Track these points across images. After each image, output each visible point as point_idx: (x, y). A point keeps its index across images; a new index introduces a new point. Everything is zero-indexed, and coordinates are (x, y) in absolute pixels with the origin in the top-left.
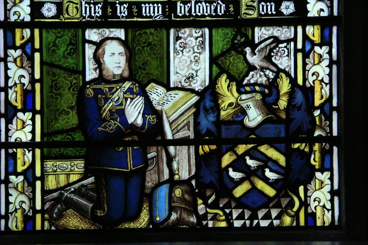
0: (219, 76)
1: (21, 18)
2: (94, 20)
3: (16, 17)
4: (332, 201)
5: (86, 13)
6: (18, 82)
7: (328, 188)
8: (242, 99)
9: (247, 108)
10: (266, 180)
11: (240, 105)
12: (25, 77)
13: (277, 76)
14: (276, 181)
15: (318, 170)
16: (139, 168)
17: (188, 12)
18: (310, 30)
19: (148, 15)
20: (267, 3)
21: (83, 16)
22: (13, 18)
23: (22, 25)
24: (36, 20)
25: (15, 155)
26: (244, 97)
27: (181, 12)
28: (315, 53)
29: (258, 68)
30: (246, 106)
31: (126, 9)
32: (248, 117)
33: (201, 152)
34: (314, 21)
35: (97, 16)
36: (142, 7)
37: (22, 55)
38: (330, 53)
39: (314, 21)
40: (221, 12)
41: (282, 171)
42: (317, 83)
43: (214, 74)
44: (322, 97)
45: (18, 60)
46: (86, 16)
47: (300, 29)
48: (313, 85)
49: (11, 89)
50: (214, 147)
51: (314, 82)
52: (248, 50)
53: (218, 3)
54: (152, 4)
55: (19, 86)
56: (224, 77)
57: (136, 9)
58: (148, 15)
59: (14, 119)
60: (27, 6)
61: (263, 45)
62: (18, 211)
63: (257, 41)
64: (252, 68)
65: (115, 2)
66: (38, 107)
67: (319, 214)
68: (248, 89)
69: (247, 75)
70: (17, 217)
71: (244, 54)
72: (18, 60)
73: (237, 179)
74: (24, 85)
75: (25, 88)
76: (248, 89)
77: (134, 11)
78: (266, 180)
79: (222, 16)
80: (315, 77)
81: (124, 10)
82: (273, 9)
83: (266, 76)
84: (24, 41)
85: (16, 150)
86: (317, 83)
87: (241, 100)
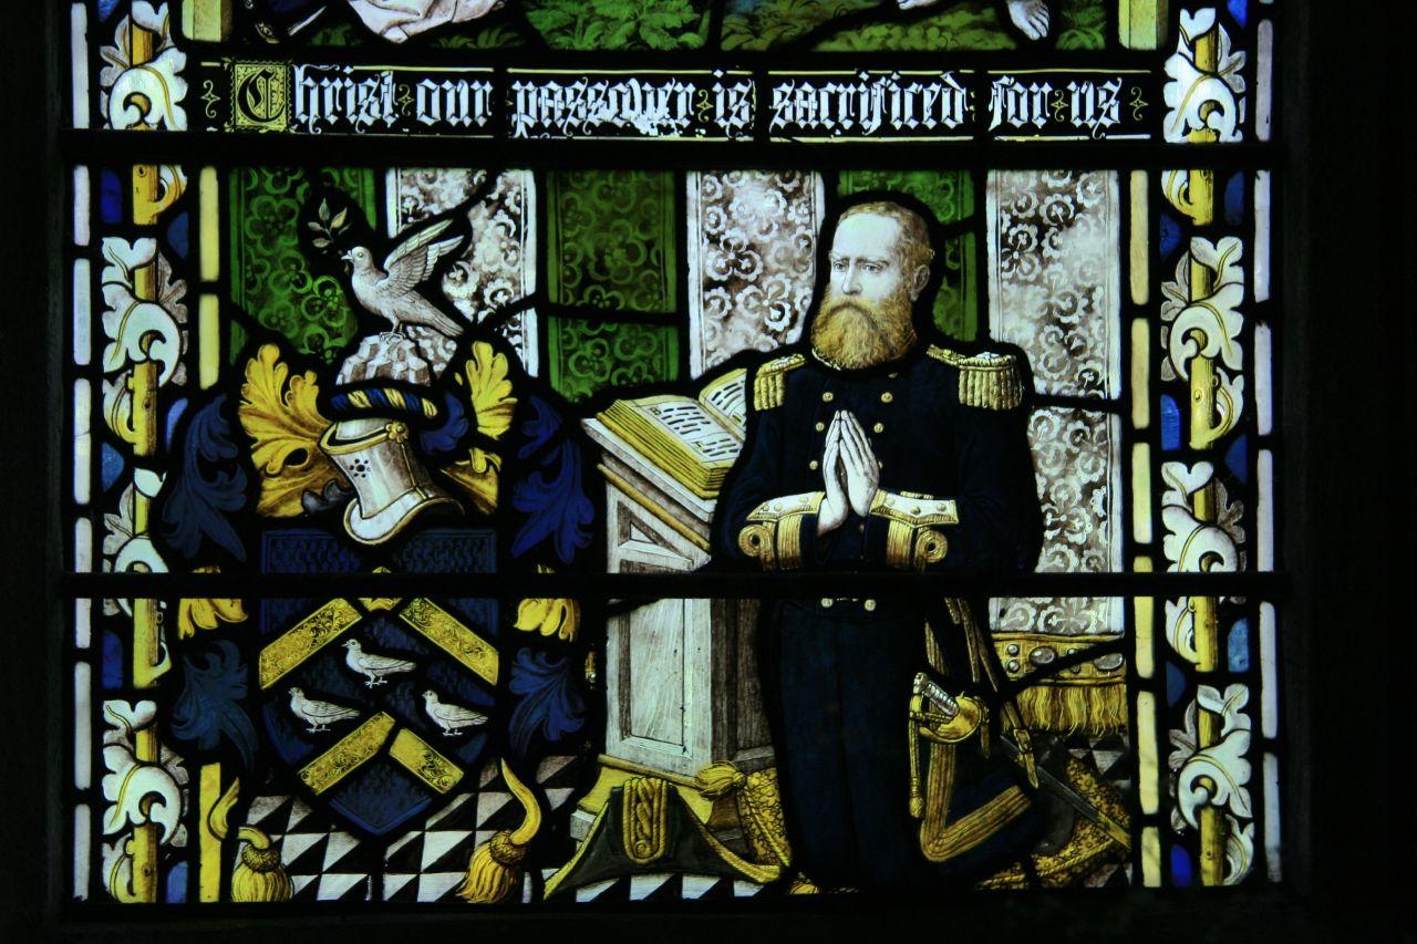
0: (251, 352)
1: (153, 119)
2: (725, 139)
3: (133, 115)
4: (1246, 340)
5: (307, 111)
6: (137, 356)
7: (1235, 295)
8: (338, 437)
9: (355, 471)
10: (429, 732)
11: (328, 458)
12: (163, 340)
13: (463, 355)
14: (469, 732)
15: (1207, 679)
16: (989, 664)
17: (335, 112)
18: (1172, 182)
19: (814, 124)
20: (443, 82)
21: (298, 121)
22: (121, 119)
23: (154, 146)
24: (1146, 137)
25: (124, 625)
26: (351, 429)
27: (428, 112)
28: (1194, 264)
29: (395, 322)
30: (353, 463)
31: (1116, 98)
32: (359, 502)
33: (185, 627)
34: (1187, 157)
35: (570, 124)
36: (516, 92)
37: (156, 258)
38: (1253, 709)
39: (1187, 157)
40: (952, 116)
41: (484, 698)
42: (1199, 366)
43: (235, 349)
44: (1216, 419)
45: (140, 275)
46: (307, 121)
47: (1139, 180)
48: (1185, 376)
49: (113, 383)
50: (232, 610)
51: (1188, 363)
52: (358, 255)
53: (945, 85)
54: (535, 84)
55: (141, 836)
56: (270, 353)
57: (213, 92)
58: (814, 124)
59: (125, 493)
60: (1175, 80)
61: (414, 242)
62: (137, 831)
63: (393, 230)
64: (371, 323)
65: (712, 76)
66: (210, 268)
67: (1207, 833)
68: (359, 399)
69: (353, 348)
70: (131, 858)
71: (344, 274)
72: (140, 275)
73: (452, 731)
74: (160, 366)
75: (163, 379)
76: (359, 399)
77: (207, 102)
78: (429, 732)
79: (959, 130)
80: (1191, 348)
81: (737, 103)
82: (479, 109)
83: (419, 352)
84: (163, 205)
85: (131, 605)
86: (1199, 366)
87: (333, 441)
